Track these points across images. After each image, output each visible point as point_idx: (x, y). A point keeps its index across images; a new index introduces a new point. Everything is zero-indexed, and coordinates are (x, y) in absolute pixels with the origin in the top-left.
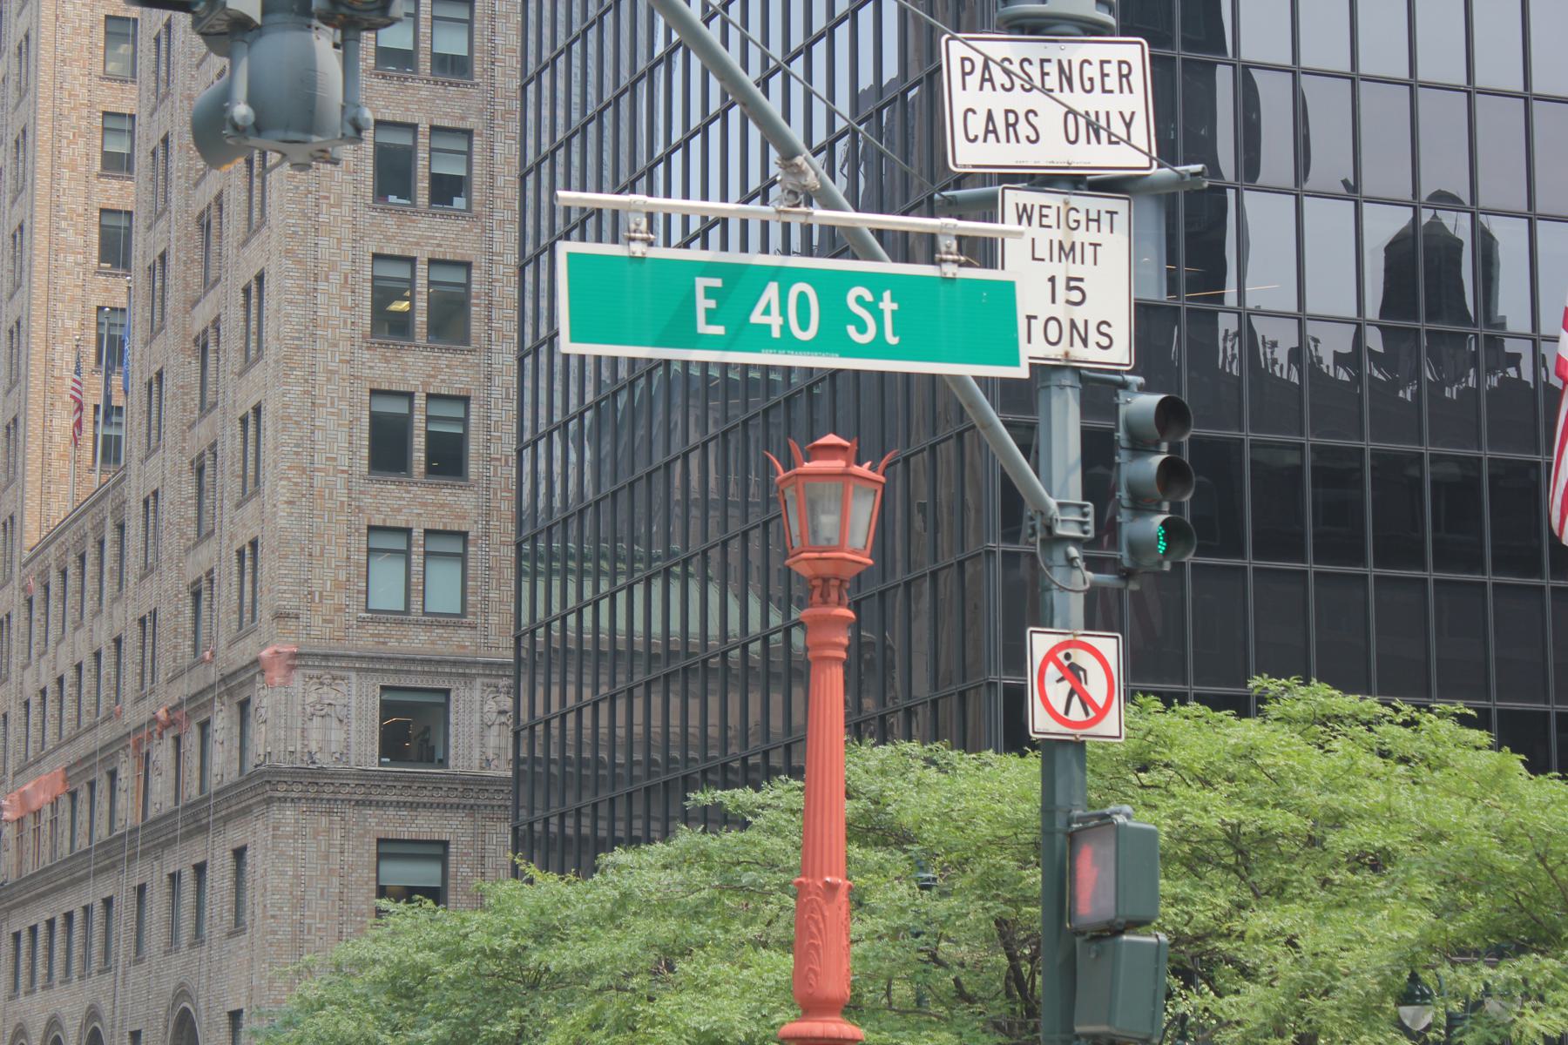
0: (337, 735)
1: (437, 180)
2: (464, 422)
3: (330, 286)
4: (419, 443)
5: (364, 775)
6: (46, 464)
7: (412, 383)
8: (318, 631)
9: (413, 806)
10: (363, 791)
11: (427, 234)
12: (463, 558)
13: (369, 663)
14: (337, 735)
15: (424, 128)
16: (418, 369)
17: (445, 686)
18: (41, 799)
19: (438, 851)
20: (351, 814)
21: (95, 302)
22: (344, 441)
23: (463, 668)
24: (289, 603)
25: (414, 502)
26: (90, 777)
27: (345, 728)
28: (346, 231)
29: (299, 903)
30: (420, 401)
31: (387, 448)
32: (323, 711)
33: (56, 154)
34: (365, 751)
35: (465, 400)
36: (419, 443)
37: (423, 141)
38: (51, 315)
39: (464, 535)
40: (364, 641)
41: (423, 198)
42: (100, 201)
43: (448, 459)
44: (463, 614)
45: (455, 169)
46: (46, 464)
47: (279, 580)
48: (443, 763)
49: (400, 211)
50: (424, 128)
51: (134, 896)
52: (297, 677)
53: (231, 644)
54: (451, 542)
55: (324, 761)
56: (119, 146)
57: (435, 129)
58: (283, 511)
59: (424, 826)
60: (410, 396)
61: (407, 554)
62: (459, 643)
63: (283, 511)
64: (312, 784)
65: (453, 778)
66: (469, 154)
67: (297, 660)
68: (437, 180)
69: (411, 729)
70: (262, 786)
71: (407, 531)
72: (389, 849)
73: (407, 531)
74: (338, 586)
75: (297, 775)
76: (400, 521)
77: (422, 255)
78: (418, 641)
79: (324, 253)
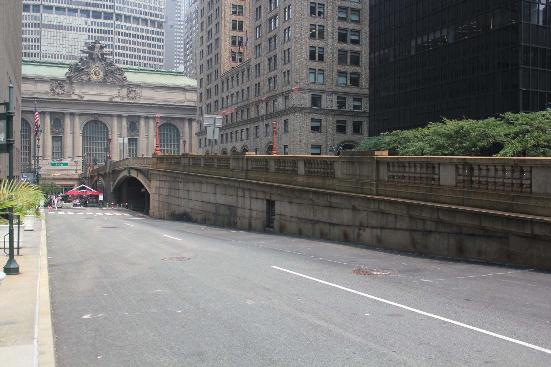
0: (305, 102)
1: (319, 12)
2: (323, 52)
3: (303, 29)
4: (317, 55)
5: (310, 108)
6: (224, 61)
7: (316, 45)
8: (302, 85)
9: (316, 113)
10: (310, 111)
11: (318, 21)
12: (323, 74)
13: (310, 90)
14: (305, 102)
15: (317, 3)
16: (317, 43)
17: (320, 94)
18: (228, 113)
19: (320, 121)
20: (308, 114)
21: (231, 35)
22: (306, 55)
23: (324, 91)
24: (298, 80)
25: (316, 65)
26: (240, 110)
27: (306, 101)
28: (306, 20)
29: (300, 128)
30: (317, 48)
31: (312, 56)
32: (303, 98)
33: (225, 11)
34: (310, 105)
35: (323, 48)
36: (317, 55)
37: (317, 6)
38: (225, 37)
39: (323, 70)
40: (309, 87)
41: (317, 15)
42: (232, 19)
43: (321, 58)
44: (323, 82)
45: (321, 11)
46: (224, 61)
47: (293, 77)
48: (321, 107)
49: (314, 17)
50: (317, 3)
51: (255, 129)
52: (299, 92)
53: (282, 87)
54: (322, 72)
55: (304, 106)
56: (235, 10)
57: (319, 4)
58: (297, 65)
59: (318, 117)
60: (315, 47)
61: (315, 73)
62: (323, 87)
63: (297, 65)
64: (302, 110)
65: (323, 109)
66: (324, 8)
67: (300, 89)
68: (319, 12)
69: (316, 100)
70: (294, 110)
71: (315, 69)
72: (313, 120)
73: (315, 69)
74: (305, 78)
75: (300, 108)
76: (314, 68)
77: (317, 24)
78: (317, 87)
79: (303, 24)
